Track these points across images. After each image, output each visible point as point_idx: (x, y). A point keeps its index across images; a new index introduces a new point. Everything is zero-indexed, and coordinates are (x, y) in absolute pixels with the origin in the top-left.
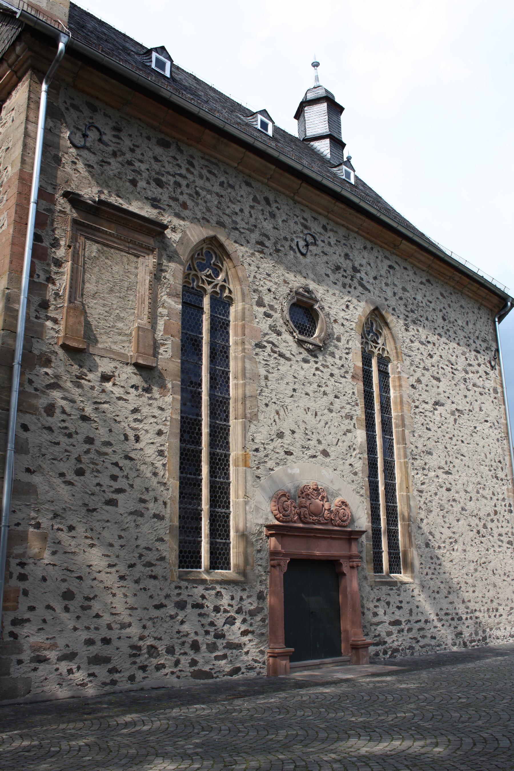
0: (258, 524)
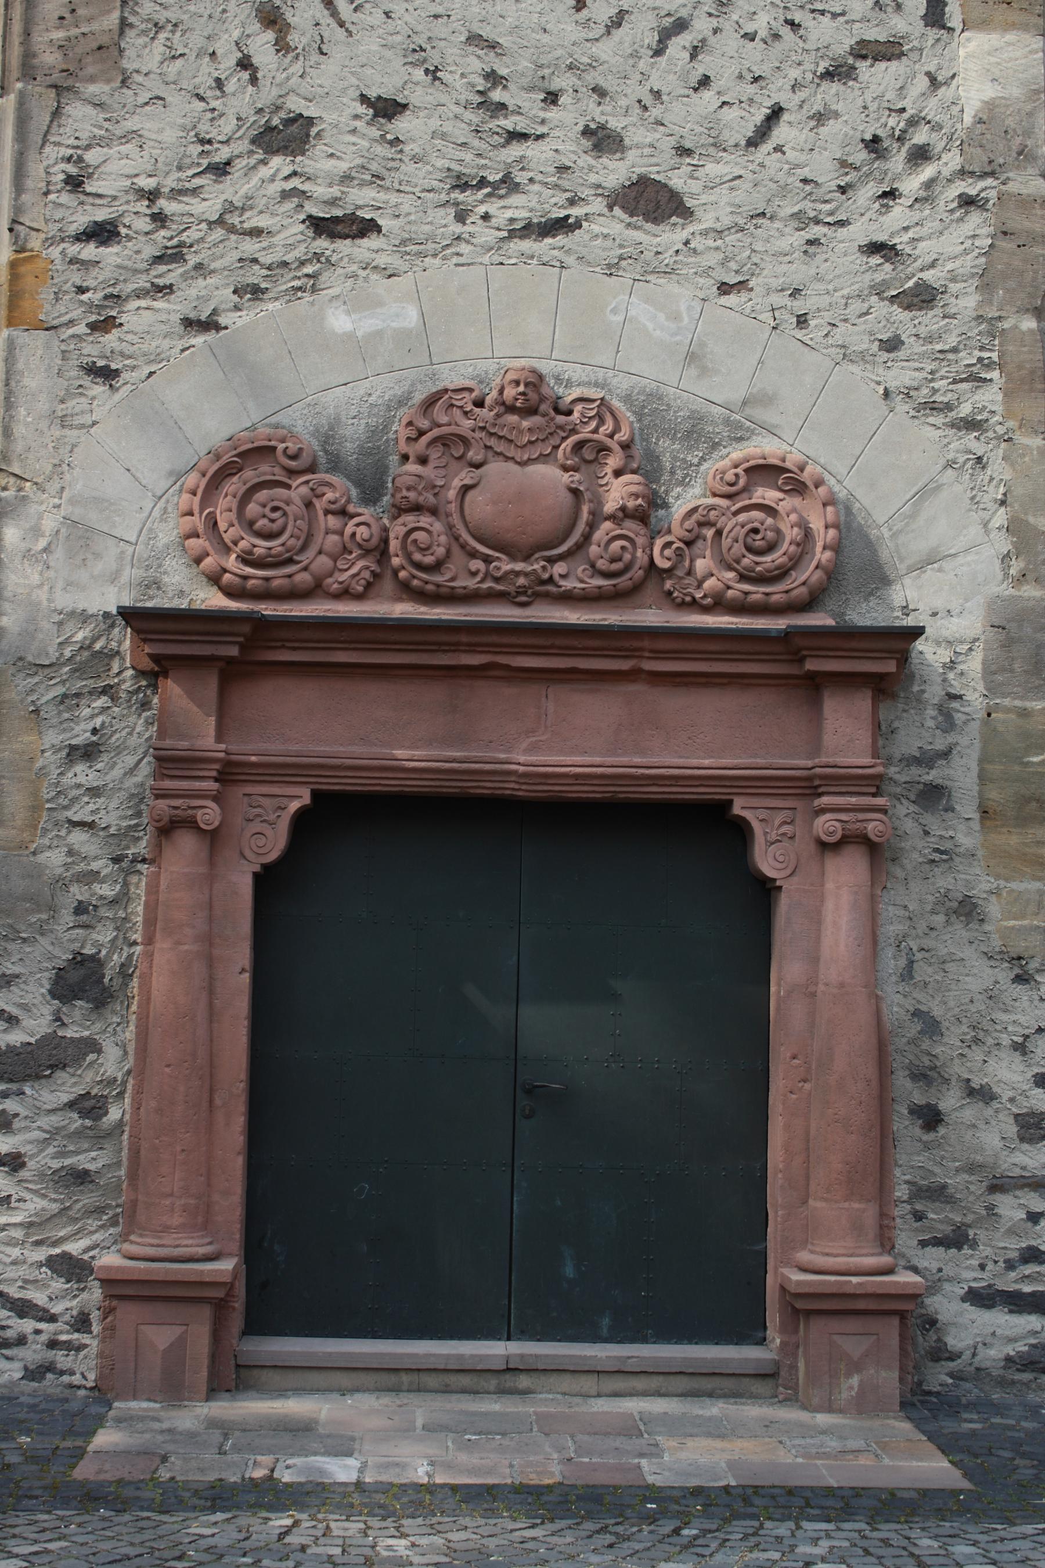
0: (84, 617)
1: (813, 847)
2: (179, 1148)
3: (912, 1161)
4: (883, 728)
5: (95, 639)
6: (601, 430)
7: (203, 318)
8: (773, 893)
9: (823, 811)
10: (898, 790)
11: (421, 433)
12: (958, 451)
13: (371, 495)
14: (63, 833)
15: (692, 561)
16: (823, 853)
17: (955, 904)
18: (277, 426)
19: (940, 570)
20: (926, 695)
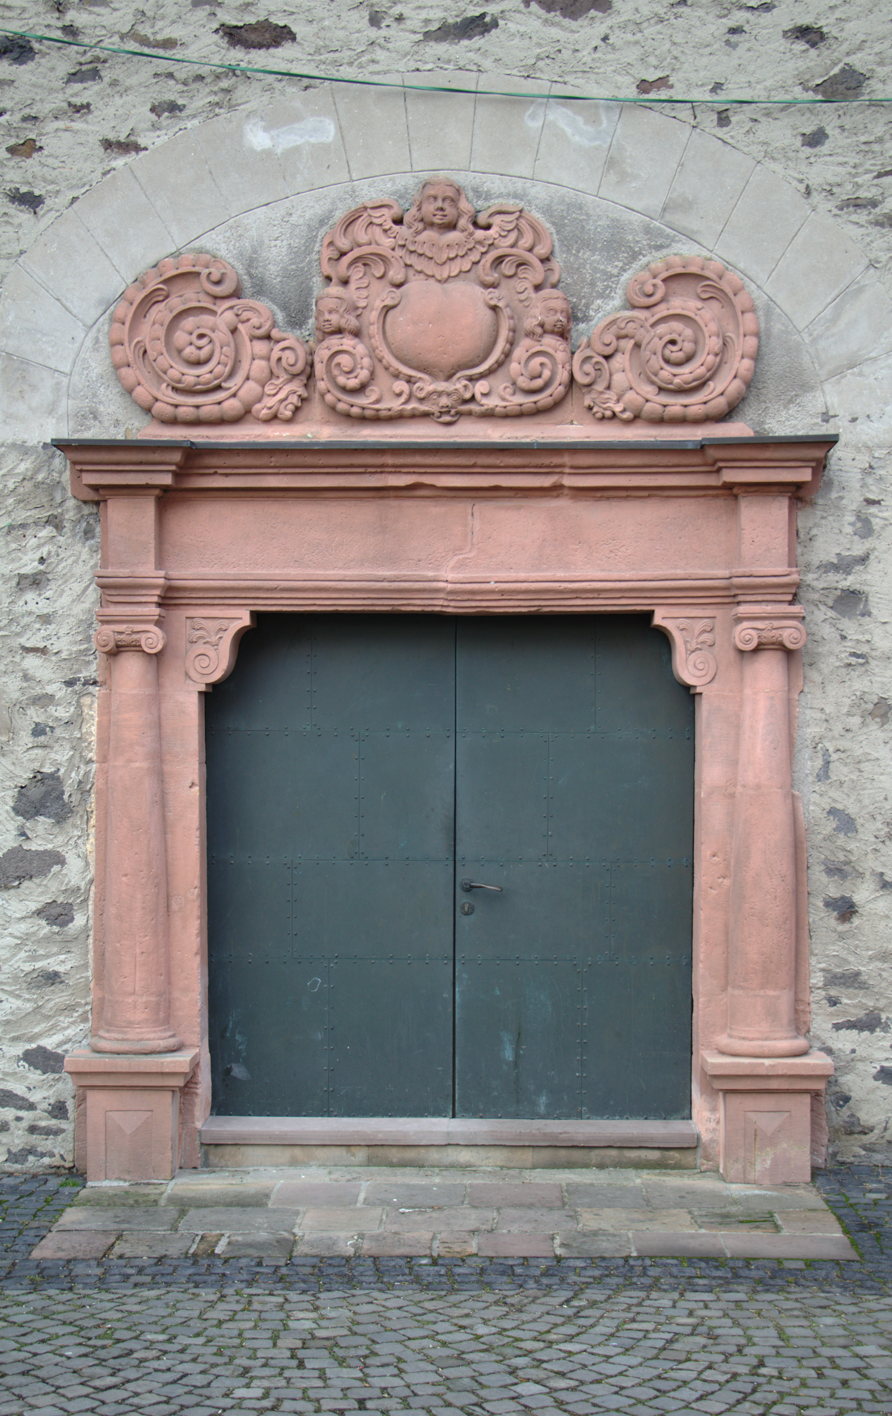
0: (23, 449)
1: (732, 654)
2: (138, 951)
3: (828, 949)
4: (802, 535)
5: (37, 471)
6: (521, 243)
7: (122, 139)
8: (697, 698)
9: (739, 620)
10: (816, 596)
11: (343, 254)
12: (881, 250)
13: (296, 321)
14: (18, 659)
15: (611, 375)
16: (742, 658)
17: (870, 706)
18: (201, 251)
19: (860, 374)
20: (844, 502)
